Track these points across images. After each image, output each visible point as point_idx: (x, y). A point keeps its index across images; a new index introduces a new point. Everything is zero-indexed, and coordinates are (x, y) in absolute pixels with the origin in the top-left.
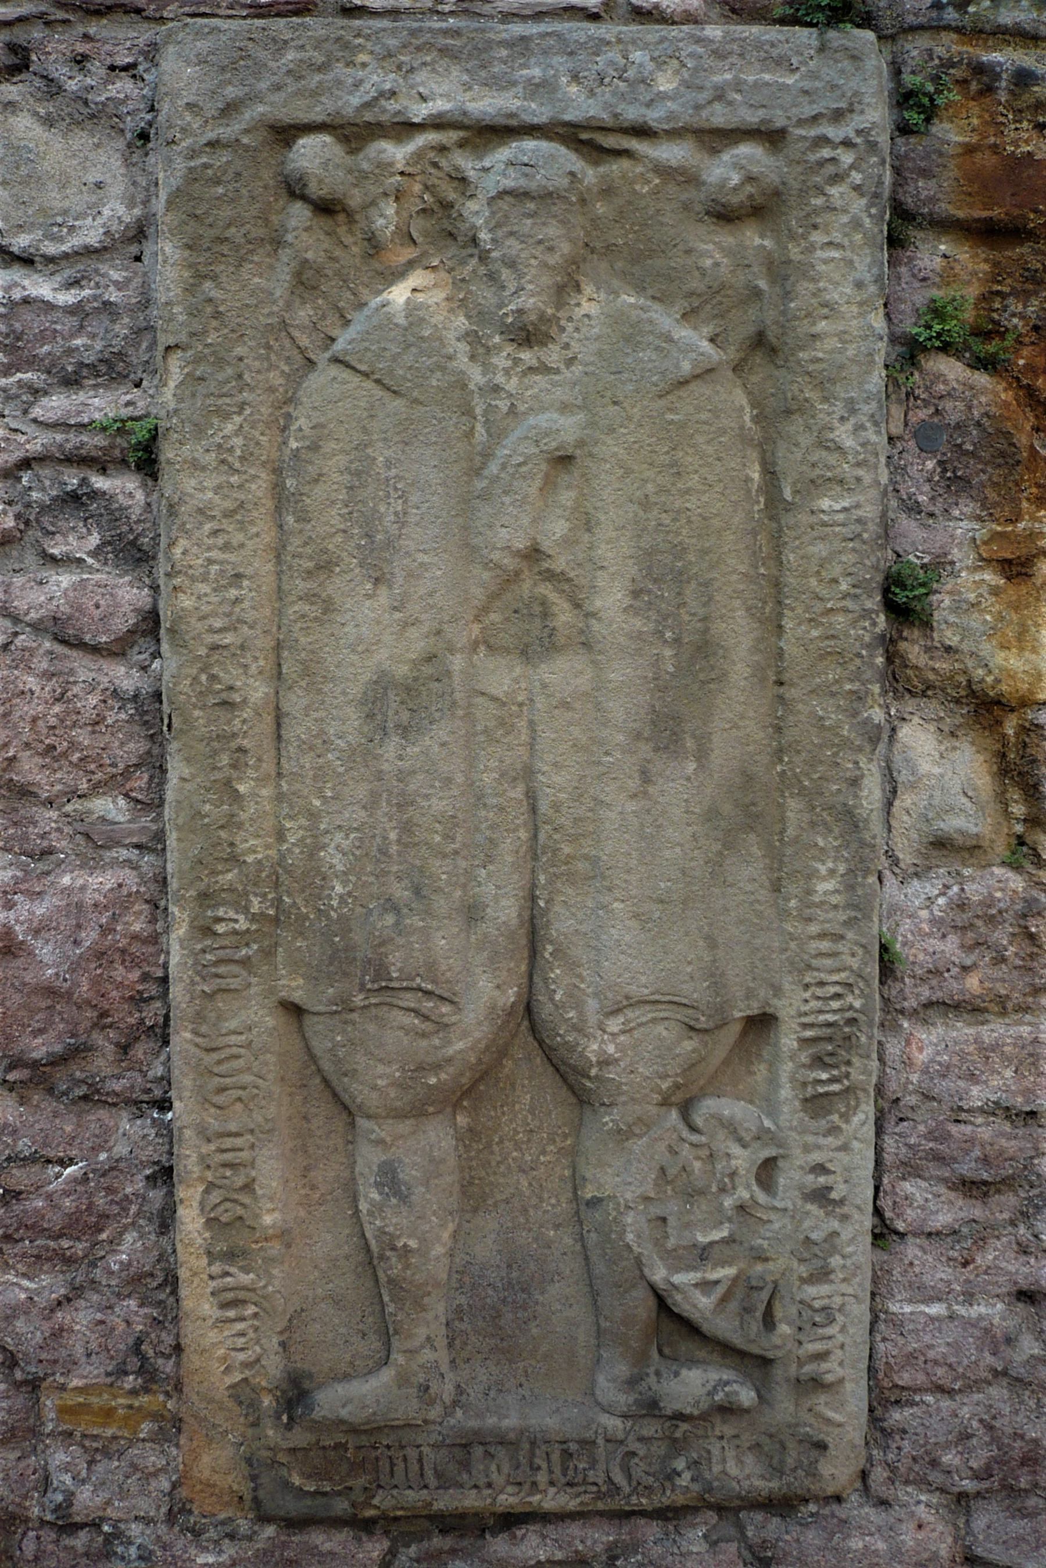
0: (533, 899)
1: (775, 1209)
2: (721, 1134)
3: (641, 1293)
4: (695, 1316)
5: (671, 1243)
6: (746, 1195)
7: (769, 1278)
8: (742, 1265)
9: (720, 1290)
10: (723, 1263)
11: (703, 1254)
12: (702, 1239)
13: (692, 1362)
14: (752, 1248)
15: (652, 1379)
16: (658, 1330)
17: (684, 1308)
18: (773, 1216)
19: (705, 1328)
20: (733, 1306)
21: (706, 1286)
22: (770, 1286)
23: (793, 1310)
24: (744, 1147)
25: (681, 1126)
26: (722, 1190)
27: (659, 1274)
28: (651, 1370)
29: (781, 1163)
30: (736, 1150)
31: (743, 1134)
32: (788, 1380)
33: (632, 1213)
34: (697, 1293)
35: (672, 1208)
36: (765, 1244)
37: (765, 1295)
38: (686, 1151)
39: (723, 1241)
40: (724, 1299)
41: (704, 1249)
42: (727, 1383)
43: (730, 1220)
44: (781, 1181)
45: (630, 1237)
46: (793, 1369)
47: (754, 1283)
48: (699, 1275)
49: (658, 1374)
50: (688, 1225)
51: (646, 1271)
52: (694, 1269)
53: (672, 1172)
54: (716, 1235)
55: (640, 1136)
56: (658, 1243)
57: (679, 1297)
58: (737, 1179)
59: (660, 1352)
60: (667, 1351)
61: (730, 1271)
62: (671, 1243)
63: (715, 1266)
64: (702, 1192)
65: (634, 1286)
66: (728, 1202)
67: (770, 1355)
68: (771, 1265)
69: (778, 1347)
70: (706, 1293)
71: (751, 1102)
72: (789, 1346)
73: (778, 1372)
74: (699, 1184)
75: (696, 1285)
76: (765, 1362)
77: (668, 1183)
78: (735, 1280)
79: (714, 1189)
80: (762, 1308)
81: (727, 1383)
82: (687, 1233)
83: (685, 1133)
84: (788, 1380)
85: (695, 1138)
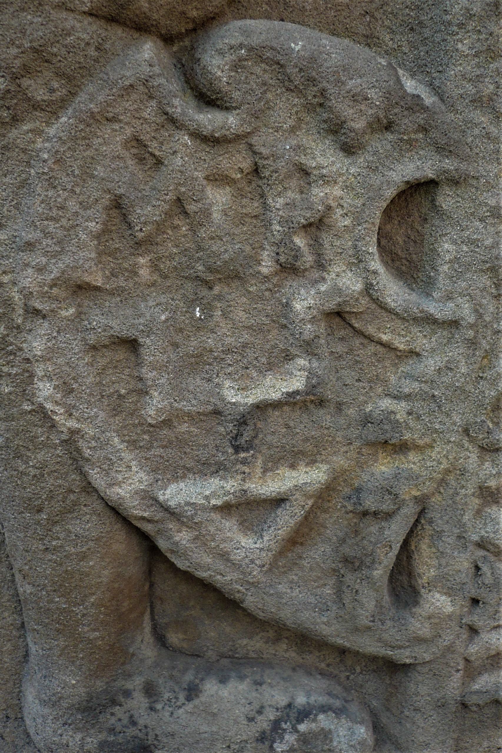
0: (84, 13)
1: (429, 321)
2: (284, 109)
3: (88, 524)
4: (226, 579)
5: (155, 406)
6: (352, 283)
7: (408, 492)
8: (340, 461)
9: (285, 521)
10: (294, 457)
11: (243, 434)
12: (236, 396)
13: (231, 664)
14: (367, 420)
15: (138, 702)
16: (151, 598)
17: (202, 562)
18: (422, 341)
19: (251, 601)
20: (318, 553)
21: (249, 510)
22: (409, 511)
23: (463, 563)
24: (349, 150)
25: (171, 85)
26: (289, 269)
27: (129, 484)
28: (137, 683)
29: (446, 199)
30: (324, 156)
31: (346, 110)
32: (441, 705)
33: (44, 328)
34: (229, 528)
35: (152, 312)
36: (400, 409)
37: (395, 531)
38: (181, 154)
39: (291, 401)
40: (295, 540)
41: (242, 422)
42: (304, 714)
43: (309, 348)
44: (447, 248)
45: (45, 390)
46: (453, 686)
47: (370, 503)
48: (231, 485)
49: (150, 691)
50: (198, 362)
51: (95, 475)
52: (219, 469)
53: (147, 213)
54: (274, 387)
55: (52, 109)
56: (123, 406)
57: (183, 537)
58: (326, 239)
59: (160, 639)
60: (174, 638)
61: (311, 476)
62: (155, 406)
63: (271, 465)
64: (233, 274)
65: (71, 509)
66: (304, 301)
67: (404, 656)
68: (412, 462)
69: (420, 640)
70: (246, 526)
71: (370, 40)
72: (447, 638)
73: (420, 689)
74: (226, 250)
75: (226, 509)
76: (392, 669)
77: (139, 245)
78: (324, 495)
79: (267, 266)
80: (387, 559)
81: (304, 714)
82: (196, 382)
83: (182, 106)
84: (441, 705)
85: (209, 120)
